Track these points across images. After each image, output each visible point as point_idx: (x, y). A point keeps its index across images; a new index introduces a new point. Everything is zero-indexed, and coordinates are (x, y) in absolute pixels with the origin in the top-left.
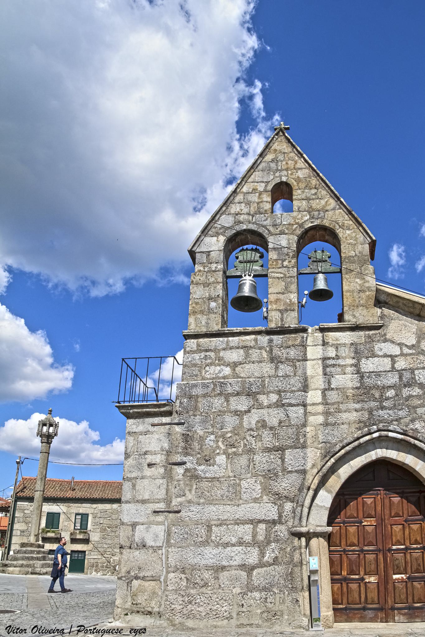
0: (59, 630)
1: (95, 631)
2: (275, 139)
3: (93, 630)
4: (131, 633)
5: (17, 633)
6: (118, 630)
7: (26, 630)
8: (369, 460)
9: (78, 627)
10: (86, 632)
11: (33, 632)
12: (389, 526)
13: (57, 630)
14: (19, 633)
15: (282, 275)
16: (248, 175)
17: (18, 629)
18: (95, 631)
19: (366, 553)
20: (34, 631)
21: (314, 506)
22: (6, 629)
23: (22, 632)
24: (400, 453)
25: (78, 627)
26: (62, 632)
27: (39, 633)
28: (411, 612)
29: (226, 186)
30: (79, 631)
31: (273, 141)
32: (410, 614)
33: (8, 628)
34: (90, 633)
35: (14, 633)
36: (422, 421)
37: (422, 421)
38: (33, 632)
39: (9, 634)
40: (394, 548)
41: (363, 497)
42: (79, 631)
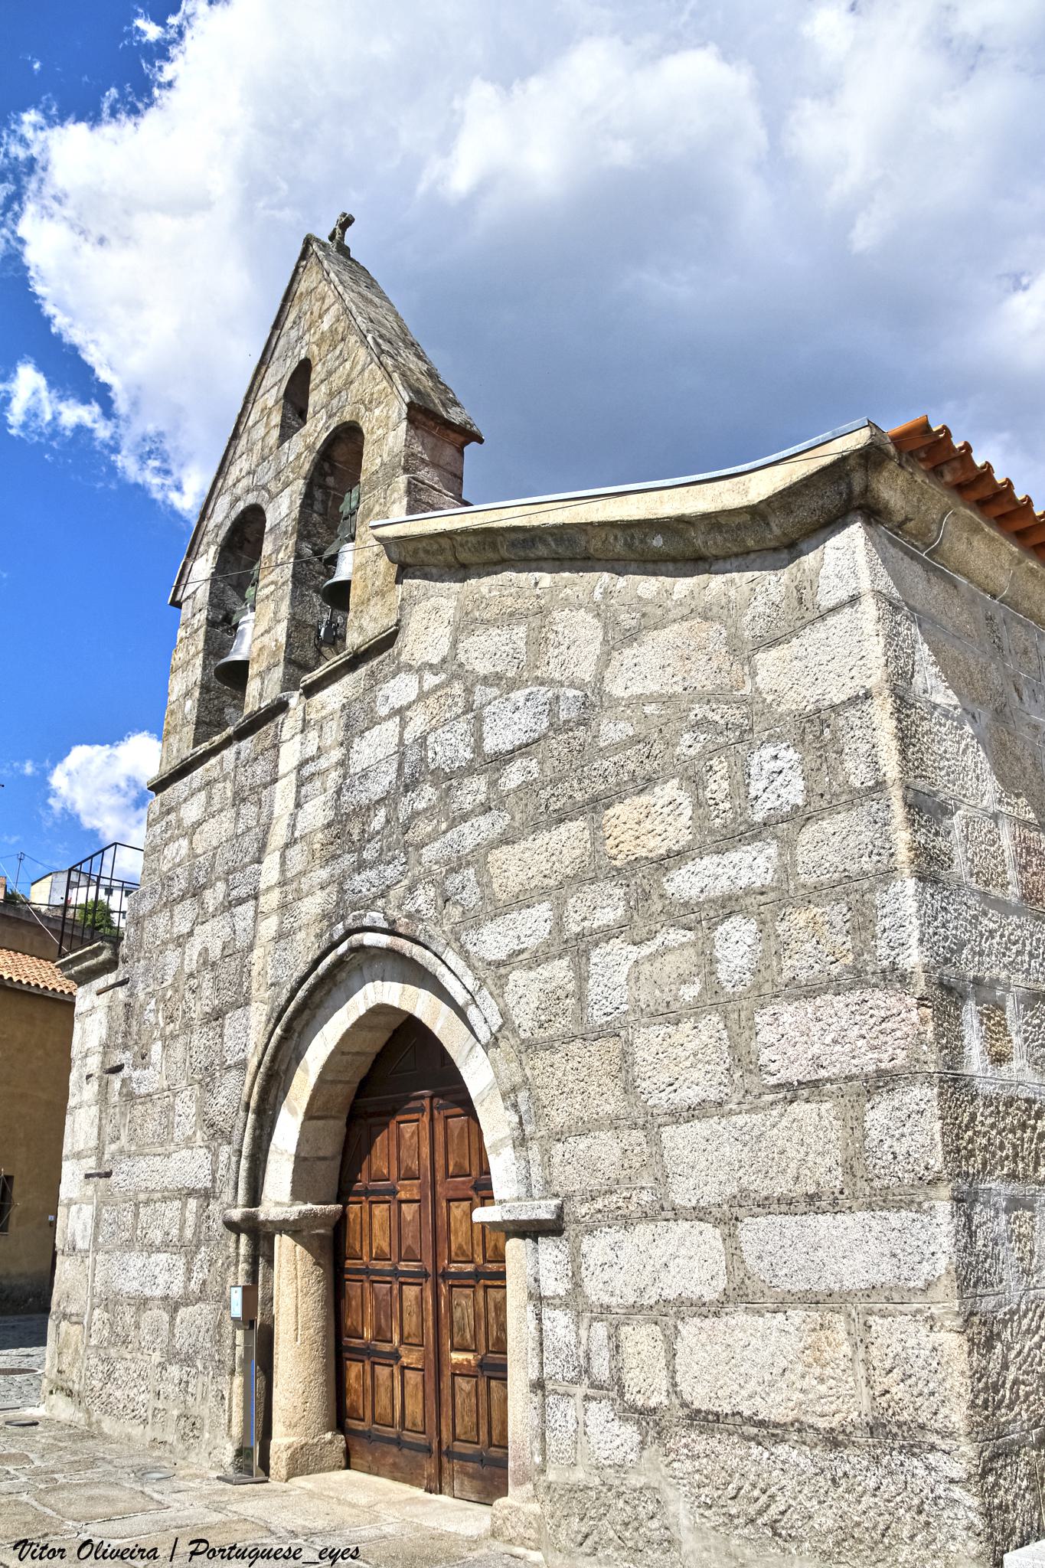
0: (144, 1550)
1: (234, 1552)
2: (301, 270)
3: (227, 1552)
4: (321, 1558)
5: (41, 1558)
6: (290, 1550)
7: (64, 1550)
8: (354, 1018)
9: (192, 1542)
10: (211, 1555)
11: (82, 1556)
12: (444, 1204)
13: (140, 1550)
14: (46, 1559)
15: (273, 587)
16: (257, 384)
17: (45, 1548)
18: (234, 1552)
19: (456, 1283)
20: (84, 1553)
21: (71, 1203)
22: (15, 1548)
23: (54, 1556)
24: (407, 986)
25: (192, 1542)
26: (153, 1554)
27: (97, 1558)
28: (486, 1471)
29: (968, 79)
30: (193, 1553)
31: (298, 278)
32: (482, 1478)
33: (20, 1547)
34: (222, 1557)
35: (33, 1558)
36: (428, 882)
37: (428, 882)
38: (82, 1556)
39: (21, 1560)
40: (453, 1270)
41: (399, 1118)
42: (193, 1553)
